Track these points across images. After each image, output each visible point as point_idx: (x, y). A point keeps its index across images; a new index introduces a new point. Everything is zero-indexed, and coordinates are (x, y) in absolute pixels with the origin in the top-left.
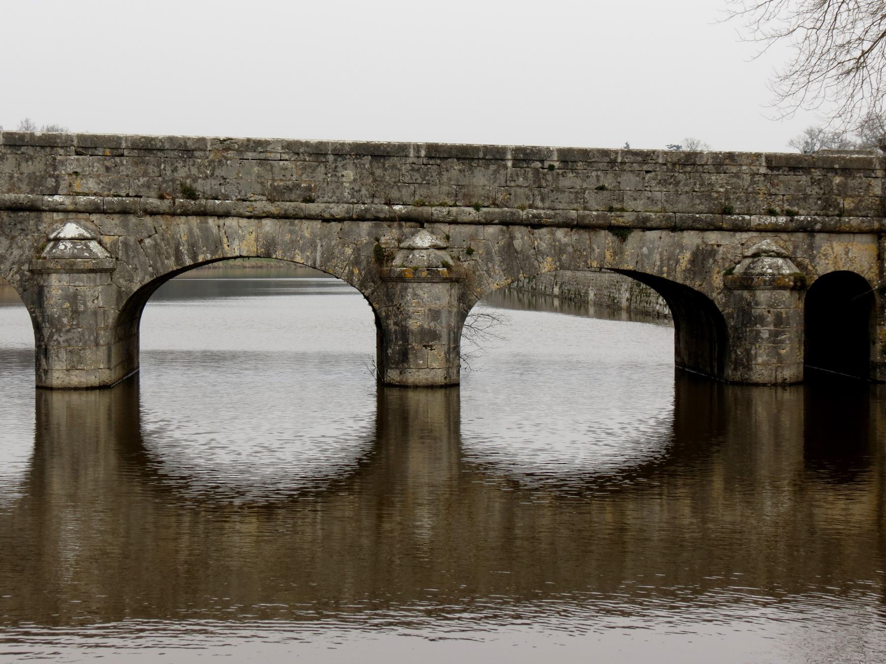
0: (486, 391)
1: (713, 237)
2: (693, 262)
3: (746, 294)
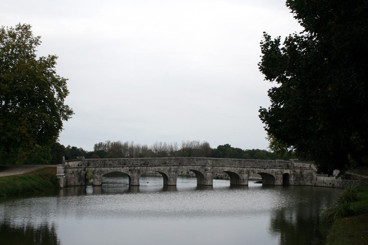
0: (168, 171)
1: (273, 169)
2: (272, 172)
3: (277, 175)
